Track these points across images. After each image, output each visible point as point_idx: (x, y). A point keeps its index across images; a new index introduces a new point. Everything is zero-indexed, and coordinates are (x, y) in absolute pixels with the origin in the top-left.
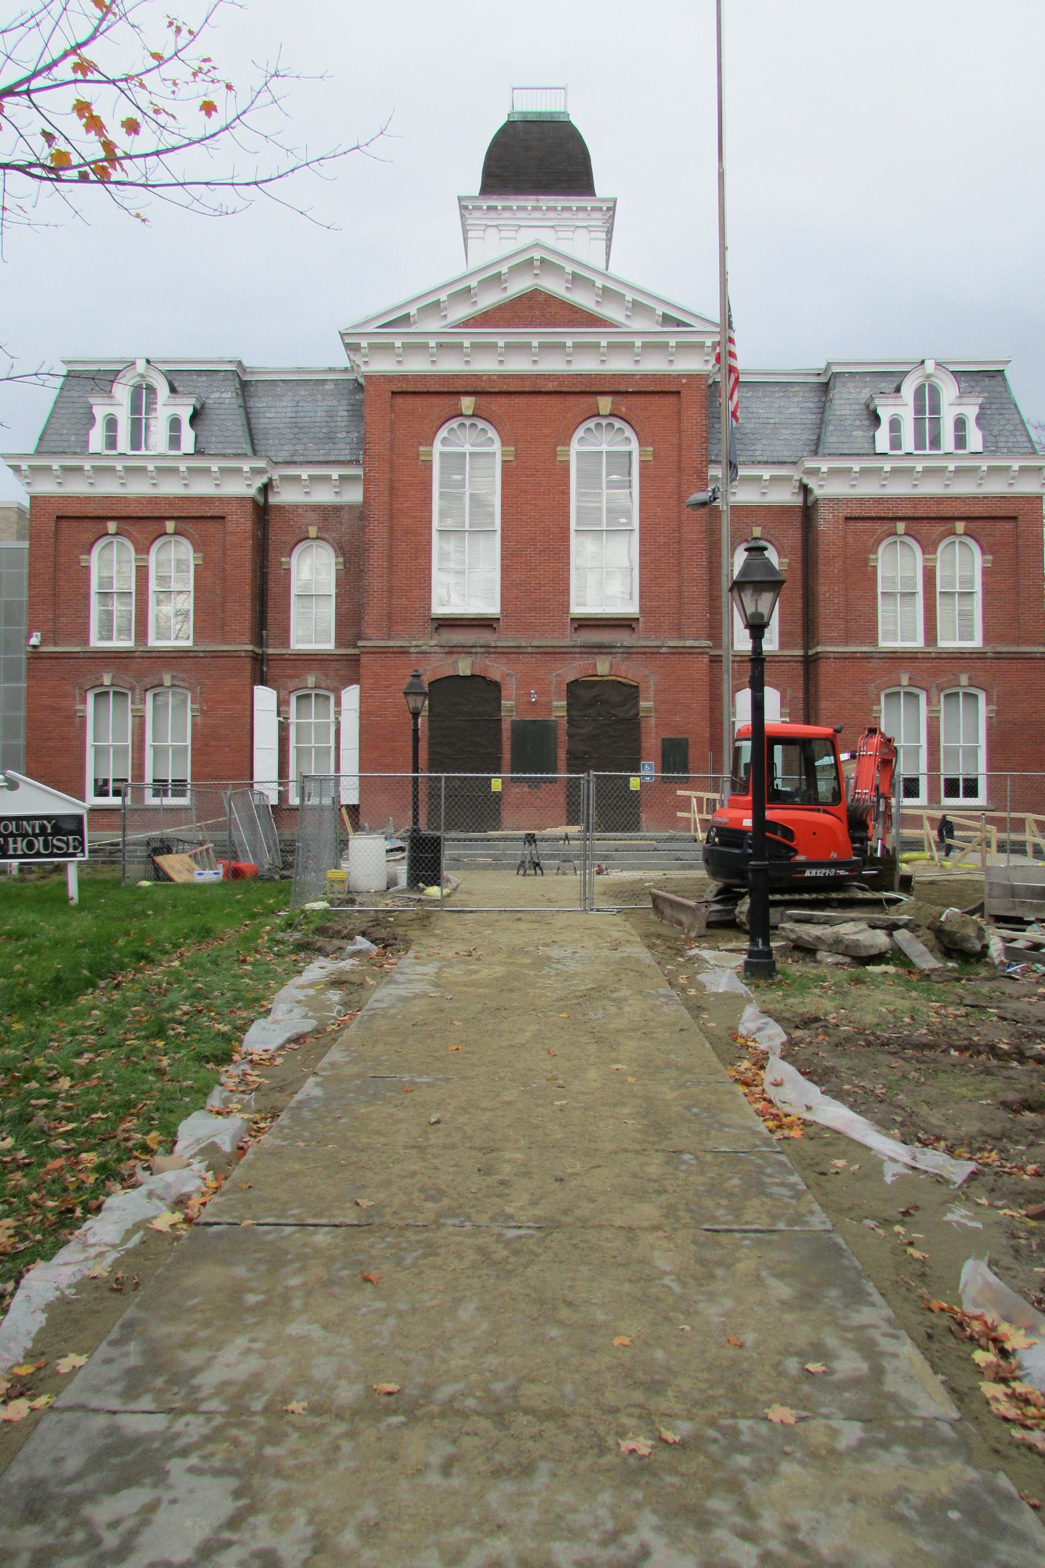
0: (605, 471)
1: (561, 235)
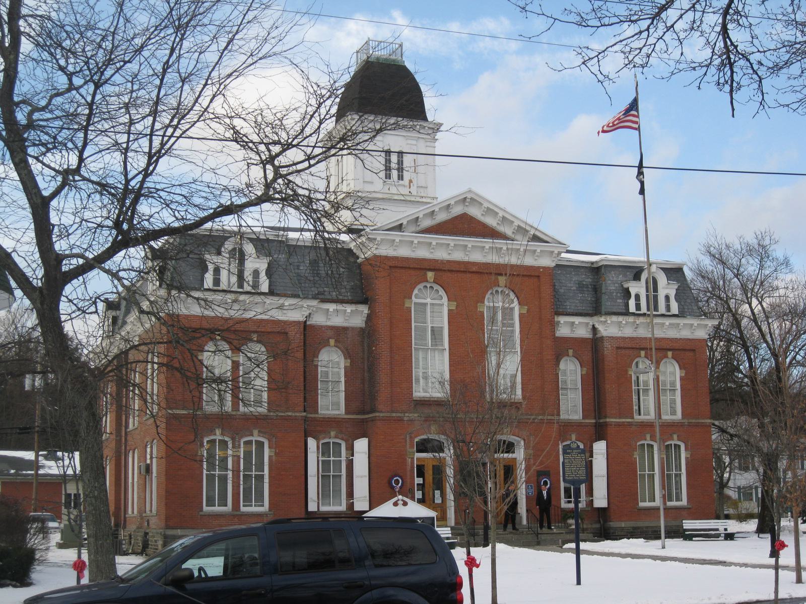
1: (410, 142)
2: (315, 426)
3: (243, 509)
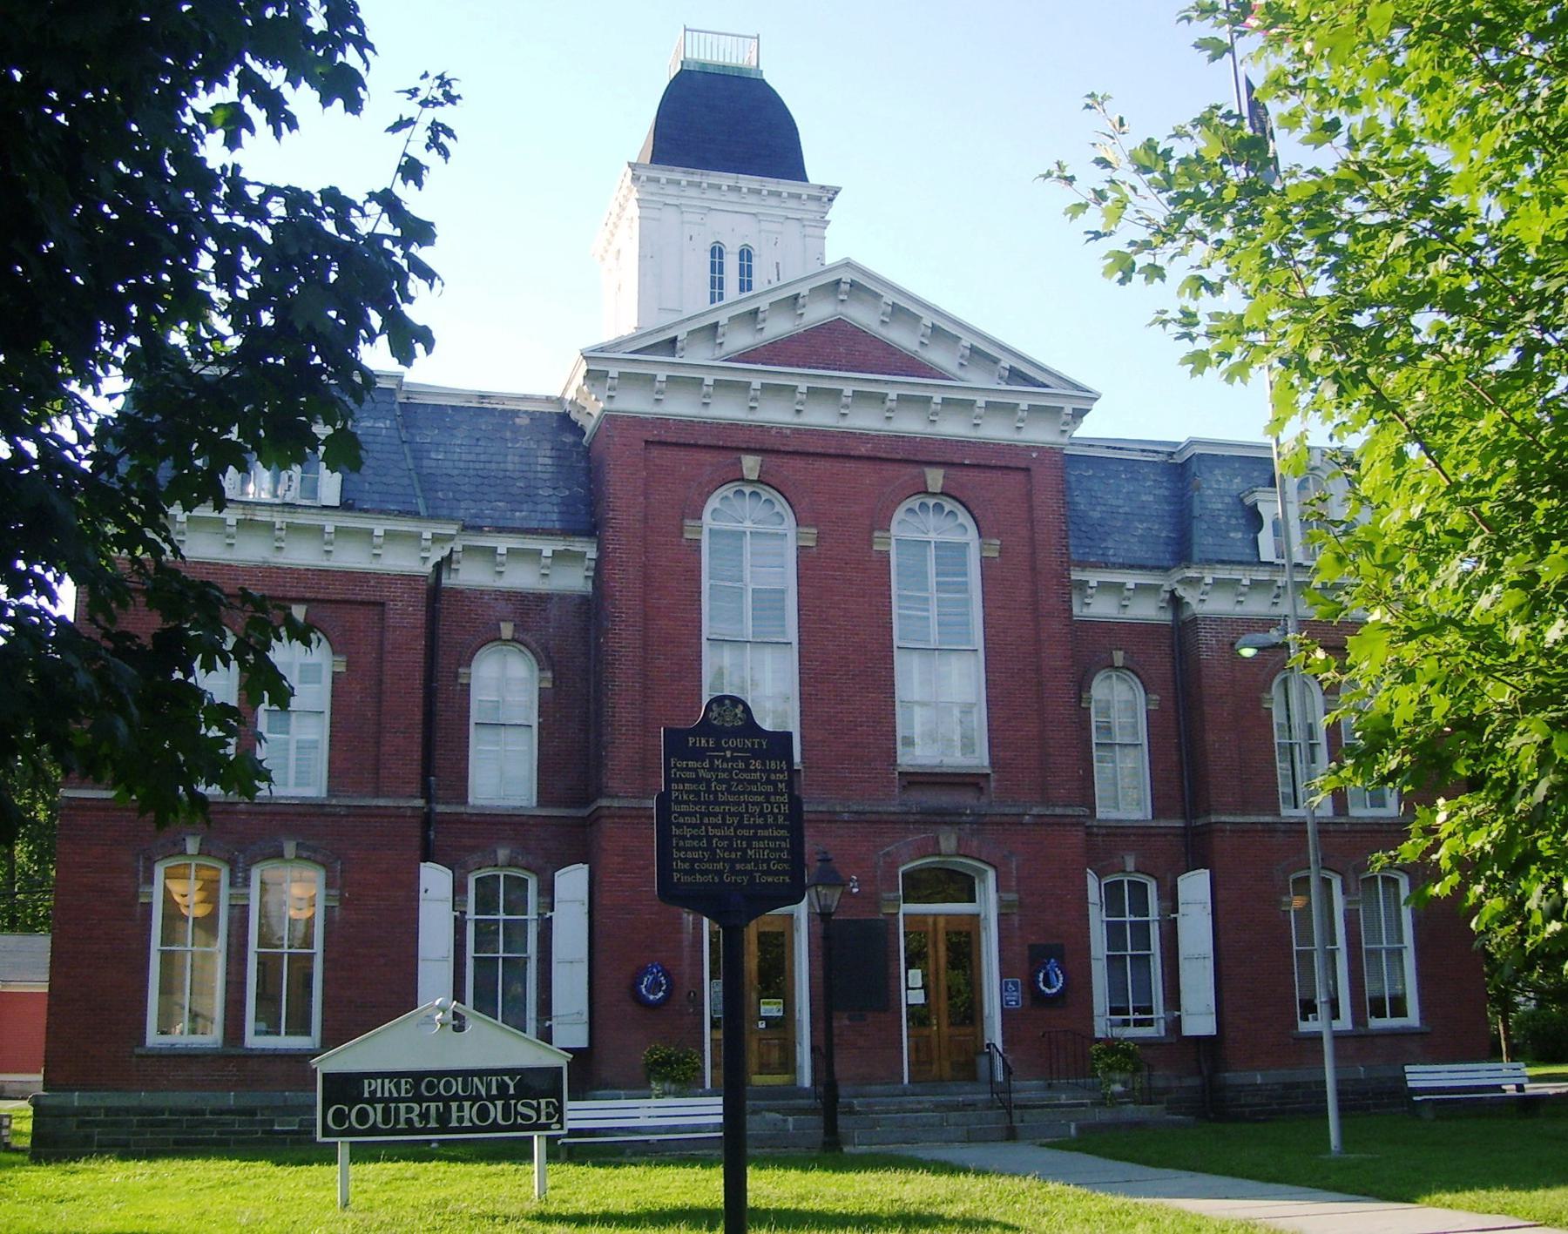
0: (936, 565)
2: (453, 834)
3: (254, 1041)
